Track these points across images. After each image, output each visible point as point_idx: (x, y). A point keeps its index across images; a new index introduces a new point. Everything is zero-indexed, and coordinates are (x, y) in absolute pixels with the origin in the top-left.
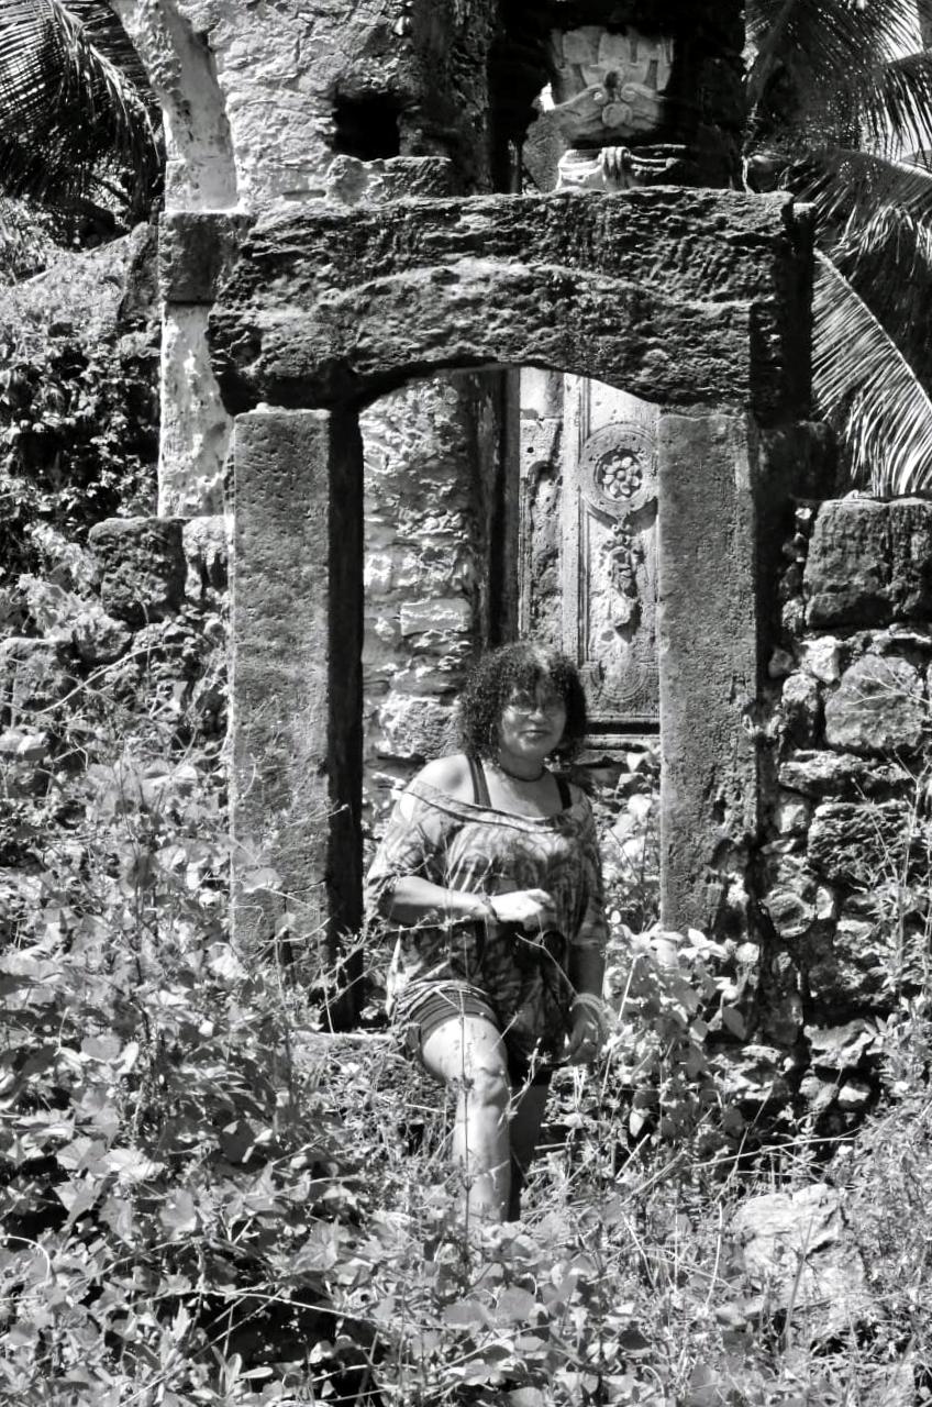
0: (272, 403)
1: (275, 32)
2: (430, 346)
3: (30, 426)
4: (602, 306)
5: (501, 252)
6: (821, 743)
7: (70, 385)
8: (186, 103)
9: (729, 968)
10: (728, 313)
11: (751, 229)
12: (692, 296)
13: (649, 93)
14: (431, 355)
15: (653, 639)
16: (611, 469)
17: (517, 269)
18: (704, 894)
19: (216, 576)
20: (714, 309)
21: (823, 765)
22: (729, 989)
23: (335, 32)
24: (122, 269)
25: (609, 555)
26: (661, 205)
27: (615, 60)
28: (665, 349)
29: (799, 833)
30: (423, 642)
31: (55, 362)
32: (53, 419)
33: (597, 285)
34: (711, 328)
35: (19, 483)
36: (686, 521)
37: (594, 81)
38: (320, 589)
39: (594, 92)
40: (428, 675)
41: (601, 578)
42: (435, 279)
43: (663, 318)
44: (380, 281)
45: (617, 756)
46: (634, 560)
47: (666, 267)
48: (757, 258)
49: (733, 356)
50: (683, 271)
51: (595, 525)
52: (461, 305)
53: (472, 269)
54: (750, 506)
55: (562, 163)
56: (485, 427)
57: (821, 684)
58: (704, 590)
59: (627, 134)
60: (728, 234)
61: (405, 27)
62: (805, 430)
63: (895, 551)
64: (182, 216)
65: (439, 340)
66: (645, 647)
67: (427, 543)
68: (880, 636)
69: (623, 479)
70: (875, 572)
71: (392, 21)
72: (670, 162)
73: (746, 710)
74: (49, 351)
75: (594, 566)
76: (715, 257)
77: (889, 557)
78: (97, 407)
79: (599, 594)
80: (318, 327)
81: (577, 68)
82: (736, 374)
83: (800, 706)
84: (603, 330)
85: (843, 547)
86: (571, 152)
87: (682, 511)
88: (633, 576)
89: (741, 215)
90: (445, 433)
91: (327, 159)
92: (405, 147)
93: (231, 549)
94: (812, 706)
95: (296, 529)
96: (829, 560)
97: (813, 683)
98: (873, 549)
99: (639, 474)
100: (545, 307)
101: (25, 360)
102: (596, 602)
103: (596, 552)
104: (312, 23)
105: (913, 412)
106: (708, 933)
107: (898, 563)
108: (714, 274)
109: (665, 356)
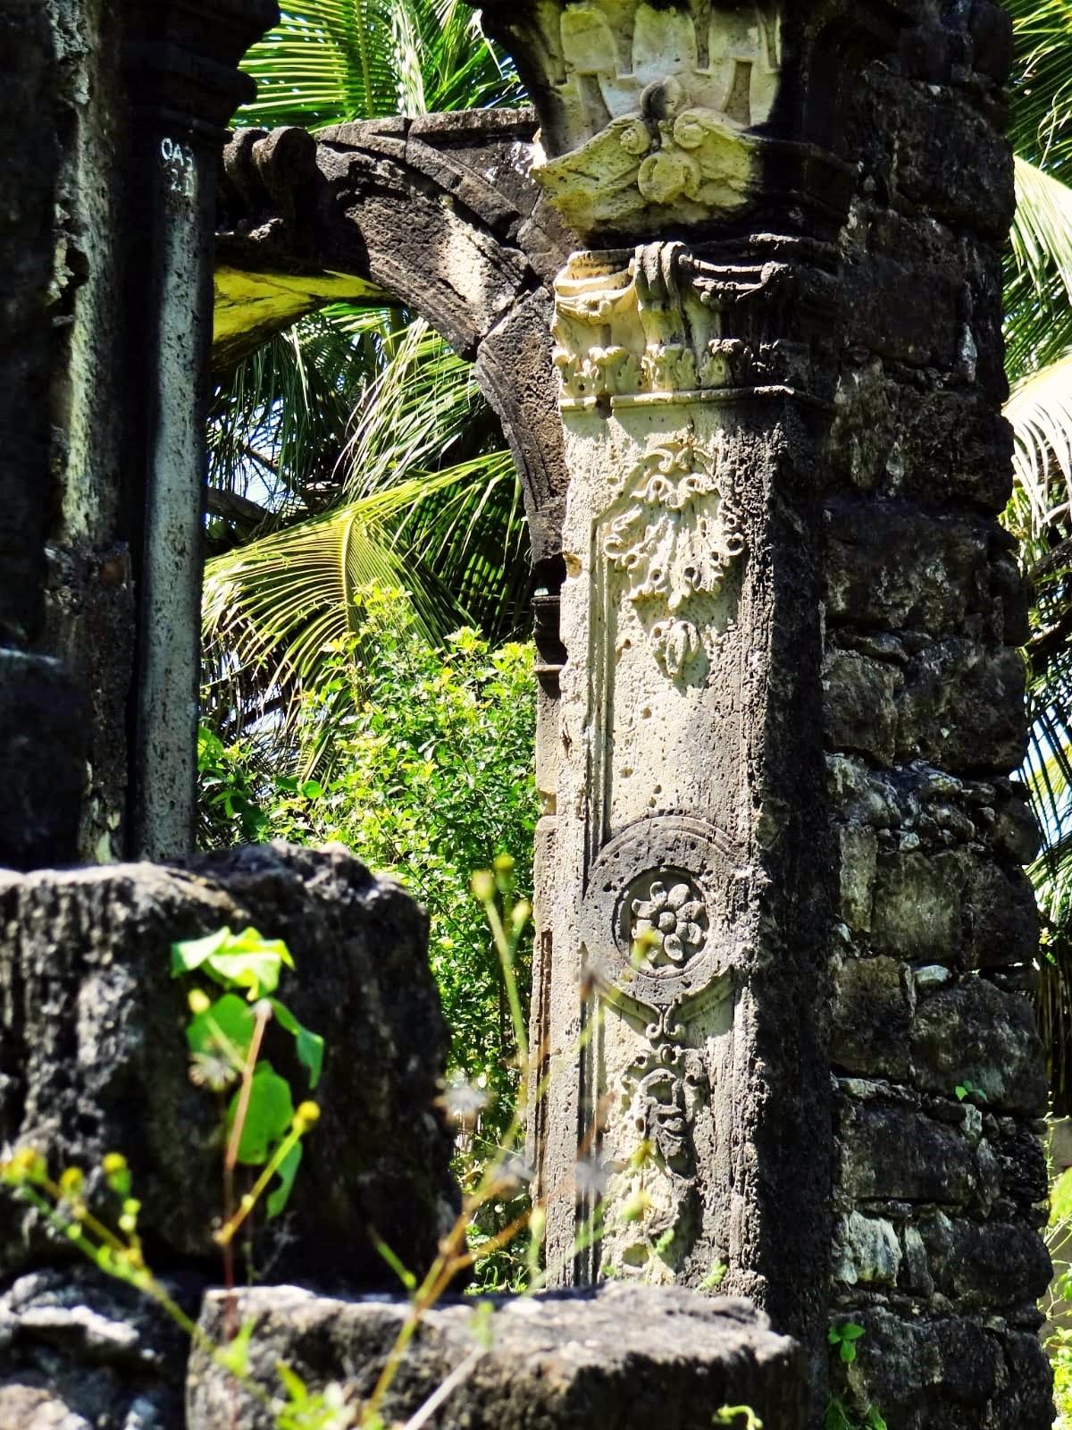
13: (730, 129)
16: (646, 909)
25: (640, 1086)
37: (623, 105)
39: (624, 126)
46: (690, 1098)
59: (693, 217)
63: (30, 1034)
72: (768, 269)
81: (590, 79)
88: (687, 1131)
103: (616, 1080)
107: (41, 1073)
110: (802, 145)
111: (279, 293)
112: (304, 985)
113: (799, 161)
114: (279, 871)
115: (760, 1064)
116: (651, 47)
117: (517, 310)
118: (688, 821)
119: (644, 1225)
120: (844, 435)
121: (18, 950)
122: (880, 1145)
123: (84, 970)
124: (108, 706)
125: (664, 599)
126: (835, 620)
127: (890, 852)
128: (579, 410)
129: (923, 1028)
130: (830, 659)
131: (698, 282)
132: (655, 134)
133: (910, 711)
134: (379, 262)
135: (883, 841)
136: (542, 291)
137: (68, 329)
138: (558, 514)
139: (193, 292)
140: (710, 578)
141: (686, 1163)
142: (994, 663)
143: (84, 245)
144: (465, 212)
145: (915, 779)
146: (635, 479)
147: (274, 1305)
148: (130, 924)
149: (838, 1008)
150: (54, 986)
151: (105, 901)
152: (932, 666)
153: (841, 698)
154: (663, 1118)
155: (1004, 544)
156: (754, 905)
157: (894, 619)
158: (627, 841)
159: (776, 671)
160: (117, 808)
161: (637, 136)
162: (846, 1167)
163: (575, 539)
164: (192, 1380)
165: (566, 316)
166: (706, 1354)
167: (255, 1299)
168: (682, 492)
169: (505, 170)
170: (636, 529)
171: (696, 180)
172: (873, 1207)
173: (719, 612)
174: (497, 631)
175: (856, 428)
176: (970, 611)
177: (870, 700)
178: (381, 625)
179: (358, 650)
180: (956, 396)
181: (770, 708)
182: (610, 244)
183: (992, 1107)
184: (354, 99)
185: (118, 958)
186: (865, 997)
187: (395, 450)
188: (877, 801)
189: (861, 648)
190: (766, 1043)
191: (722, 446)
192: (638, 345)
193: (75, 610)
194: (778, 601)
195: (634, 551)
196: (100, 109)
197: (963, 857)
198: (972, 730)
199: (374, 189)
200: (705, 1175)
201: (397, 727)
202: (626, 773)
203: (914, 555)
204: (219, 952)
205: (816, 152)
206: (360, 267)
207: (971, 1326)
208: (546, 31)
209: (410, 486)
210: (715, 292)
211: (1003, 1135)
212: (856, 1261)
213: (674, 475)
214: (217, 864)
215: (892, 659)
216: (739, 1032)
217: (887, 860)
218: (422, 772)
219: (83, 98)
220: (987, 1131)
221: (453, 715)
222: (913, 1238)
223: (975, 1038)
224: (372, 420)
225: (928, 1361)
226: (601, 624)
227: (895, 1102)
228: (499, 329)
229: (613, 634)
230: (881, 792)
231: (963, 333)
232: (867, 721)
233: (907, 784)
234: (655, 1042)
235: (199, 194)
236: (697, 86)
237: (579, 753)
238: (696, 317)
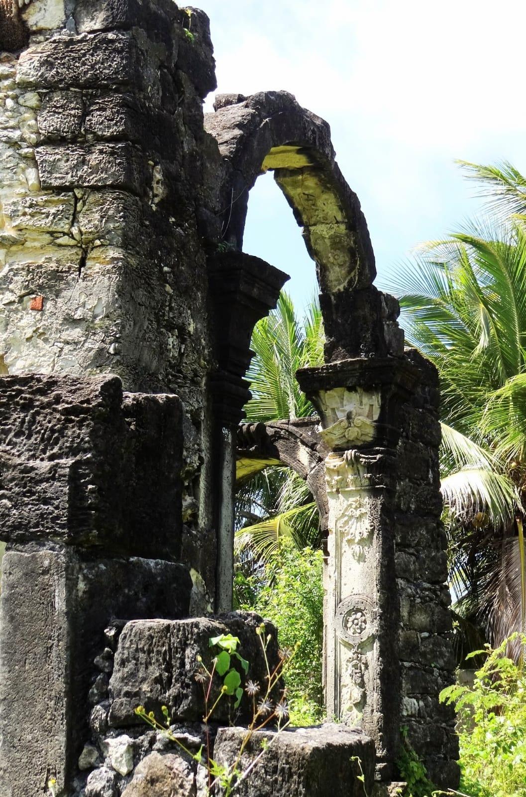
1: (41, 354)
11: (76, 402)
12: (34, 457)
13: (368, 421)
15: (372, 711)
16: (351, 619)
23: (75, 353)
25: (350, 665)
26: (17, 387)
28: (10, 499)
34: (41, 481)
37: (342, 416)
39: (342, 421)
41: (346, 679)
46: (363, 668)
47: (17, 435)
48: (80, 425)
49: (56, 502)
50: (29, 437)
51: (344, 650)
54: (65, 626)
57: (118, 776)
58: (28, 695)
59: (359, 444)
60: (60, 407)
61: (115, 349)
63: (173, 662)
68: (162, 735)
69: (357, 624)
70: (158, 680)
71: (108, 346)
72: (378, 456)
75: (343, 671)
76: (50, 425)
77: (169, 668)
79: (345, 686)
81: (333, 409)
82: (58, 517)
86: (330, 453)
87: (16, 629)
88: (362, 676)
96: (126, 670)
97: (111, 774)
98: (158, 660)
99: (365, 622)
102: (344, 690)
103: (344, 663)
104: (62, 349)
107: (176, 672)
108: (50, 438)
109: (9, 504)
110: (386, 425)
111: (258, 464)
112: (244, 648)
113: (386, 429)
114: (238, 618)
115: (380, 659)
116: (348, 401)
117: (317, 467)
118: (361, 597)
119: (352, 701)
120: (399, 497)
121: (170, 641)
122: (412, 679)
123: (186, 645)
124: (210, 571)
125: (354, 540)
126: (397, 544)
127: (413, 604)
128: (332, 492)
129: (423, 649)
130: (396, 554)
131: (361, 460)
132: (350, 423)
133: (417, 567)
134: (282, 456)
135: (411, 601)
136: (323, 462)
137: (199, 476)
138: (327, 519)
139: (231, 466)
140: (365, 535)
141: (362, 685)
142: (439, 554)
143: (203, 455)
144: (303, 443)
145: (419, 584)
146: (346, 510)
147: (236, 732)
148: (198, 634)
149: (401, 644)
150: (179, 650)
151: (192, 627)
152: (423, 556)
153: (399, 564)
154: (356, 673)
155: (441, 524)
156: (378, 618)
157: (413, 544)
158: (345, 602)
159: (383, 558)
160: (213, 597)
161: (345, 424)
162: (404, 685)
163: (331, 525)
164: (215, 752)
165: (328, 469)
166: (348, 743)
167: (232, 730)
168: (358, 513)
169: (313, 432)
170: (346, 523)
171: (360, 434)
172: (411, 695)
173: (368, 543)
174: (316, 547)
175: (402, 496)
176: (432, 541)
177: (407, 565)
178: (286, 546)
179: (281, 554)
180: (428, 487)
181: (381, 567)
182: (339, 450)
183: (441, 669)
184: (280, 414)
185: (195, 642)
186: (407, 641)
187: (291, 500)
188: (409, 591)
189: (405, 552)
190: (382, 653)
191: (368, 501)
192: (346, 476)
193: (201, 547)
194: (383, 540)
195: (346, 528)
196: (207, 422)
197: (432, 604)
198: (434, 572)
199: (280, 437)
200: (367, 688)
201: (291, 572)
202: (345, 585)
203: (417, 528)
204: (221, 640)
205: (390, 426)
206: (278, 457)
207: (437, 726)
208: (322, 398)
209: (295, 510)
210: (365, 462)
211: (444, 676)
212: (407, 709)
213: (356, 508)
214: (222, 617)
215: (412, 554)
216: (375, 651)
217: (412, 605)
218: (297, 585)
219: (202, 418)
220: (440, 675)
221: (305, 569)
222: (421, 703)
223: (436, 651)
224: (284, 494)
225: (426, 735)
226: (338, 547)
227: (416, 668)
228: (312, 472)
229: (341, 548)
230: (410, 588)
231: (428, 471)
232: (406, 570)
233: (417, 586)
234: (354, 654)
235: (233, 441)
236: (360, 411)
237: (333, 579)
238: (361, 469)
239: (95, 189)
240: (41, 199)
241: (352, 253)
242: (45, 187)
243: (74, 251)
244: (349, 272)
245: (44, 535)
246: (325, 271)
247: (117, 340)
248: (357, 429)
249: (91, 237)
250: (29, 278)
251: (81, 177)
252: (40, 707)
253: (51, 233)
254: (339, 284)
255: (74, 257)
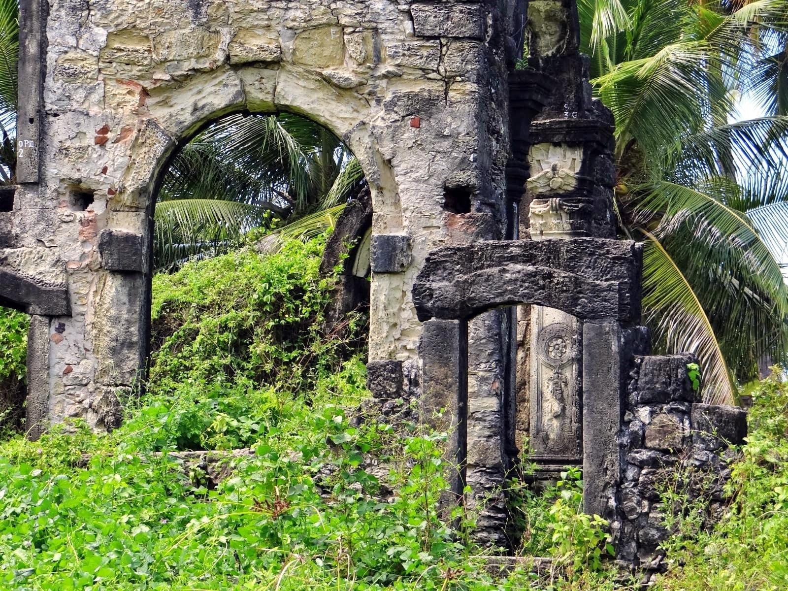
0: (437, 317)
2: (497, 296)
3: (279, 322)
4: (563, 282)
5: (525, 262)
6: (643, 446)
7: (298, 302)
8: (382, 188)
9: (609, 530)
10: (610, 286)
11: (619, 254)
14: (498, 300)
15: (571, 422)
16: (552, 345)
17: (531, 268)
18: (599, 502)
19: (414, 383)
20: (605, 284)
21: (644, 455)
22: (609, 538)
24: (322, 248)
27: (556, 158)
29: (635, 480)
30: (479, 415)
31: (290, 291)
32: (290, 318)
33: (561, 275)
35: (274, 348)
36: (594, 363)
37: (547, 169)
38: (455, 388)
40: (481, 429)
42: (500, 271)
43: (586, 287)
44: (479, 272)
45: (555, 474)
47: (587, 268)
50: (594, 269)
52: (510, 282)
53: (516, 268)
54: (618, 358)
55: (531, 205)
56: (504, 326)
57: (644, 424)
59: (561, 192)
62: (639, 329)
64: (381, 237)
65: (501, 294)
66: (567, 426)
67: (481, 374)
68: (666, 407)
72: (580, 205)
73: (616, 434)
74: (288, 286)
75: (545, 388)
77: (670, 377)
78: (310, 313)
80: (455, 289)
82: (613, 308)
83: (636, 432)
84: (563, 291)
85: (652, 373)
88: (562, 393)
89: (615, 249)
90: (489, 328)
91: (441, 213)
92: (473, 209)
93: (421, 372)
94: (641, 433)
95: (446, 365)
100: (541, 282)
101: (277, 291)
103: (545, 382)
105: (697, 319)
106: (601, 516)
107: (673, 379)
165: (534, 214)
239: (456, 39)
240: (415, 43)
241: (563, 25)
242: (416, 35)
243: (441, 83)
244: (558, 41)
245: (605, 316)
246: (536, 37)
247: (475, 152)
248: (560, 180)
249: (454, 74)
250: (409, 103)
251: (447, 30)
252: (606, 394)
253: (423, 70)
254: (548, 50)
255: (441, 89)
